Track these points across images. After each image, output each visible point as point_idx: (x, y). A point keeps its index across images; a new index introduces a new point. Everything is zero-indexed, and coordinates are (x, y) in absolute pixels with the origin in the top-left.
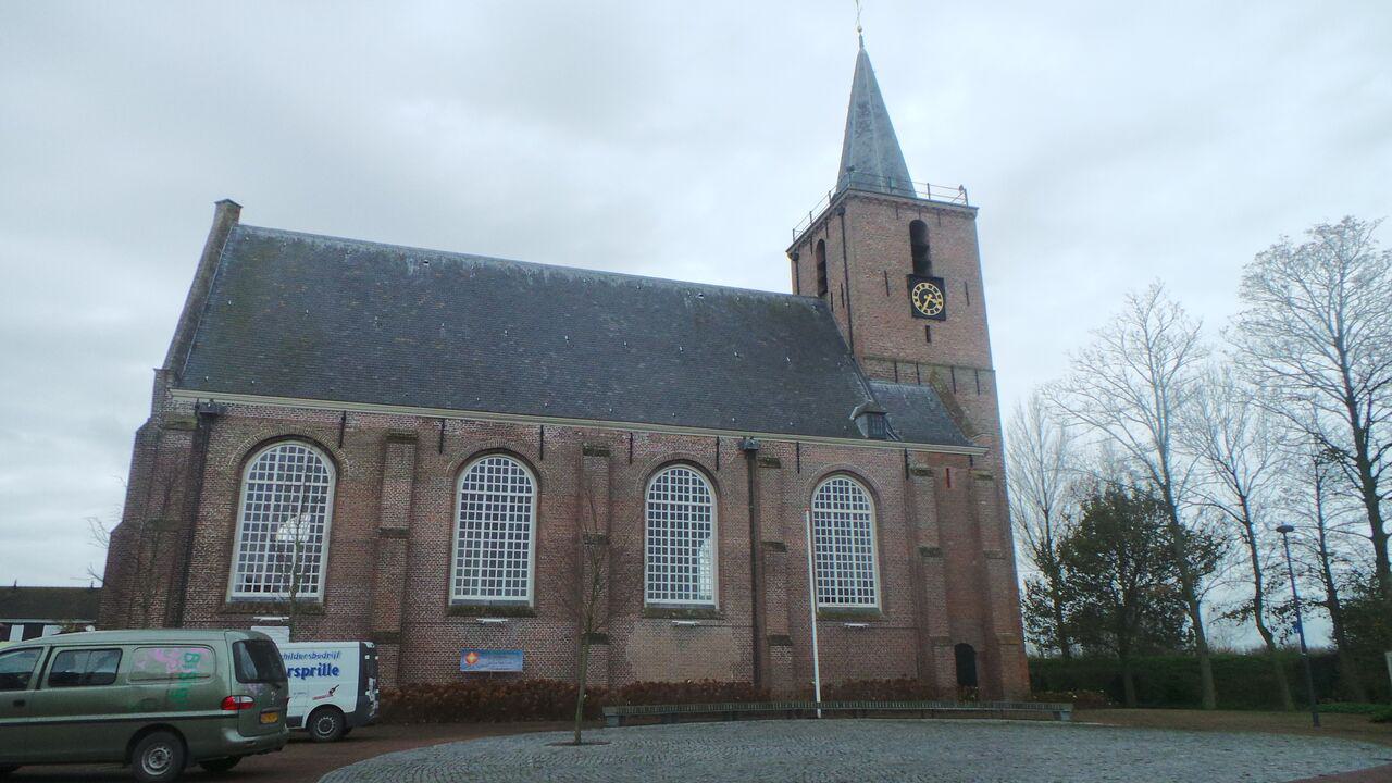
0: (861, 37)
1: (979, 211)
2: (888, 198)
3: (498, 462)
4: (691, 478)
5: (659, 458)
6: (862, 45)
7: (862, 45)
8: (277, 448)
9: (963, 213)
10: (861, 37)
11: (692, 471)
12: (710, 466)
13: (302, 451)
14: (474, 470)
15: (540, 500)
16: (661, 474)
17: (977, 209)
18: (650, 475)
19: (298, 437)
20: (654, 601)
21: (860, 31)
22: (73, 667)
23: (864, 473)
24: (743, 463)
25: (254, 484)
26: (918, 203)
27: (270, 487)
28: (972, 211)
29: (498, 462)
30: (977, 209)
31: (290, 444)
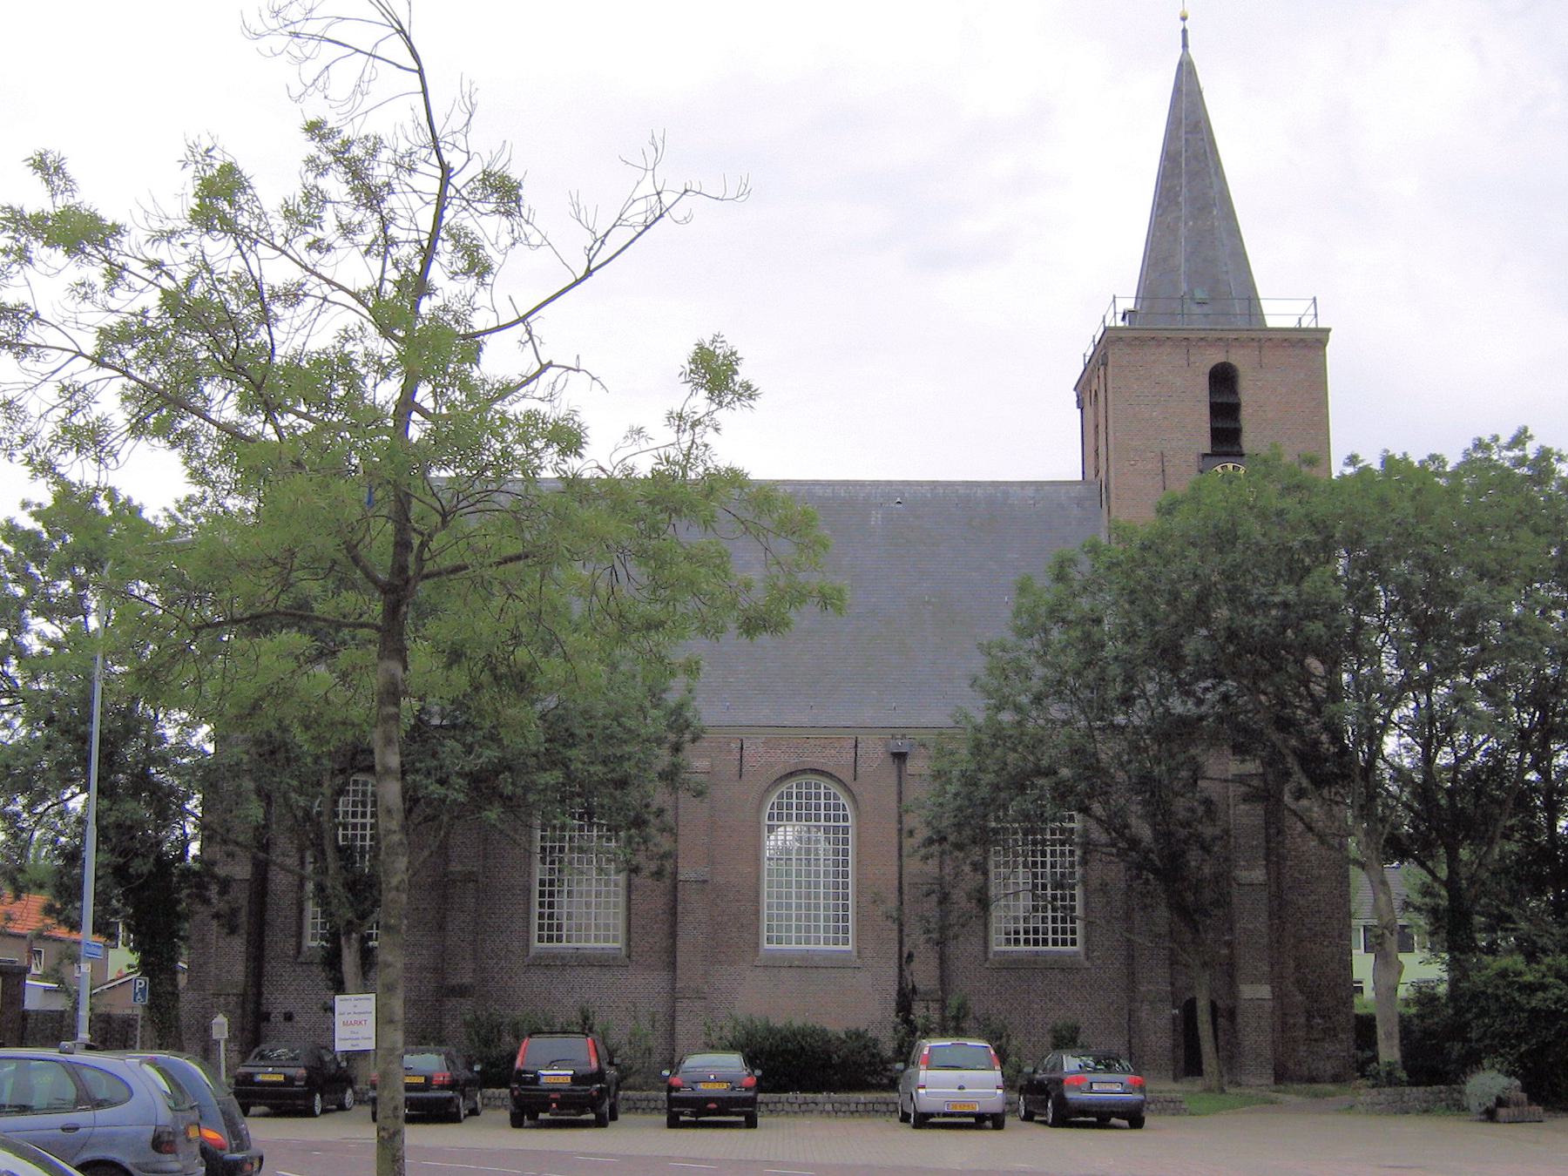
0: (1184, 31)
1: (1331, 334)
2: (1222, 335)
3: (808, 786)
4: (822, 791)
5: (780, 770)
6: (1185, 45)
7: (1185, 45)
8: (792, 786)
9: (1302, 340)
10: (1184, 31)
11: (824, 782)
12: (847, 777)
13: (818, 787)
14: (781, 796)
15: (858, 828)
16: (784, 788)
17: (1328, 331)
18: (768, 791)
19: (804, 771)
20: (774, 946)
21: (1184, 19)
22: (1418, 949)
23: (811, 761)
24: (891, 768)
25: (357, 824)
26: (1272, 336)
27: (364, 826)
28: (1319, 336)
29: (808, 786)
30: (1328, 331)
31: (803, 779)
